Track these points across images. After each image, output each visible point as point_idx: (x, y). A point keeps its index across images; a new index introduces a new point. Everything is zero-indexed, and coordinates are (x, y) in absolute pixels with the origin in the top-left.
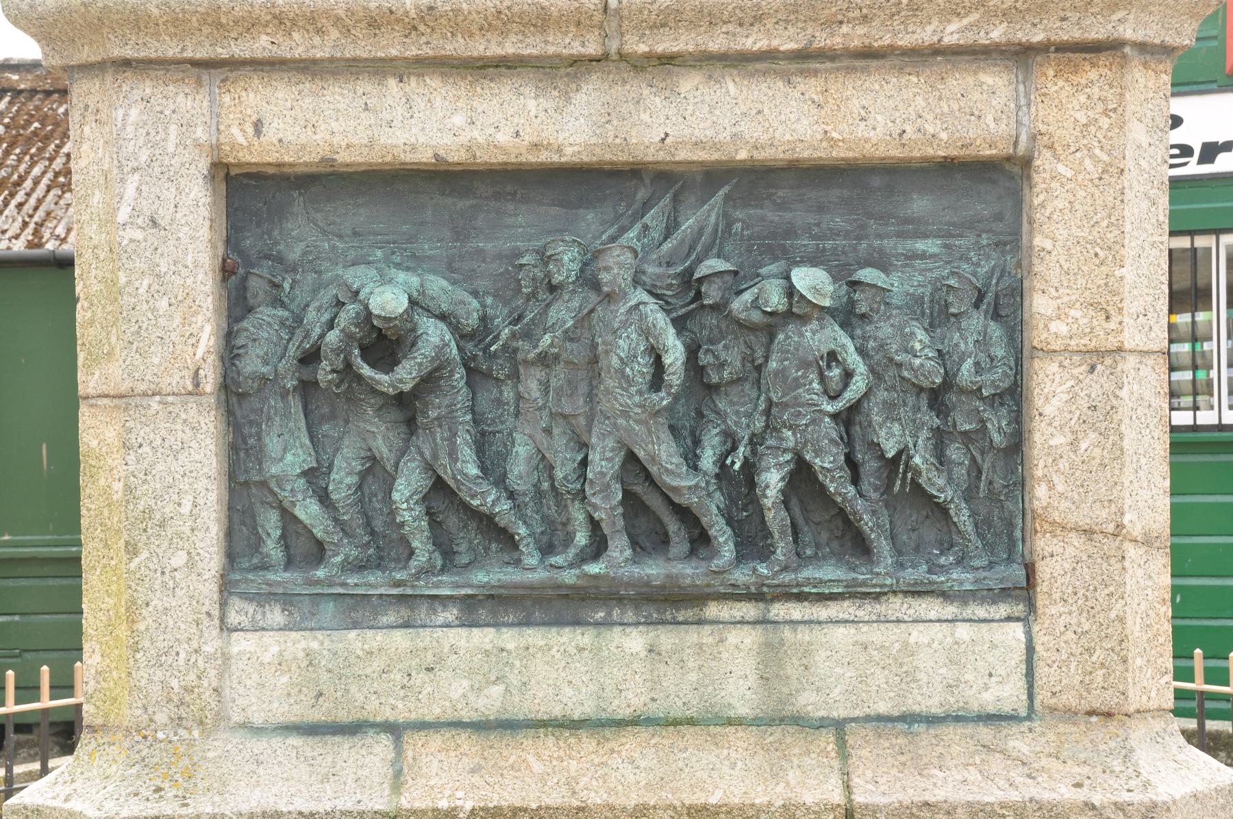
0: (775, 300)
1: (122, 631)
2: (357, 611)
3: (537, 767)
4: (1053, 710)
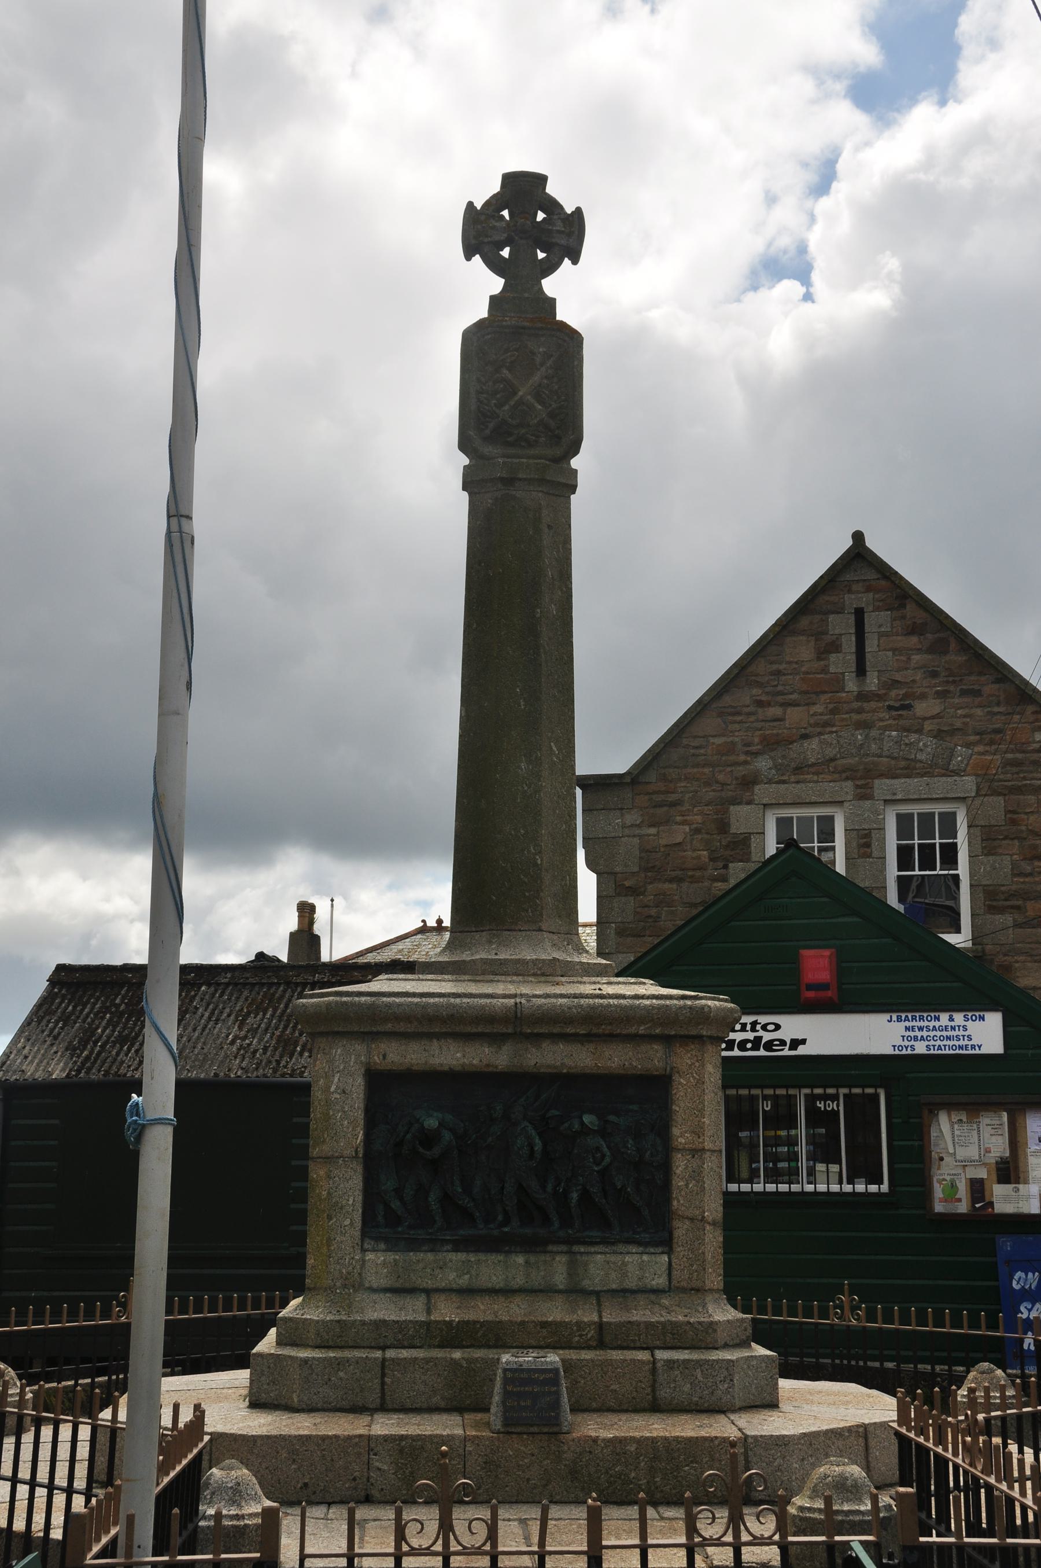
0: (577, 1126)
1: (325, 1250)
2: (413, 1245)
3: (482, 1307)
4: (678, 1288)
